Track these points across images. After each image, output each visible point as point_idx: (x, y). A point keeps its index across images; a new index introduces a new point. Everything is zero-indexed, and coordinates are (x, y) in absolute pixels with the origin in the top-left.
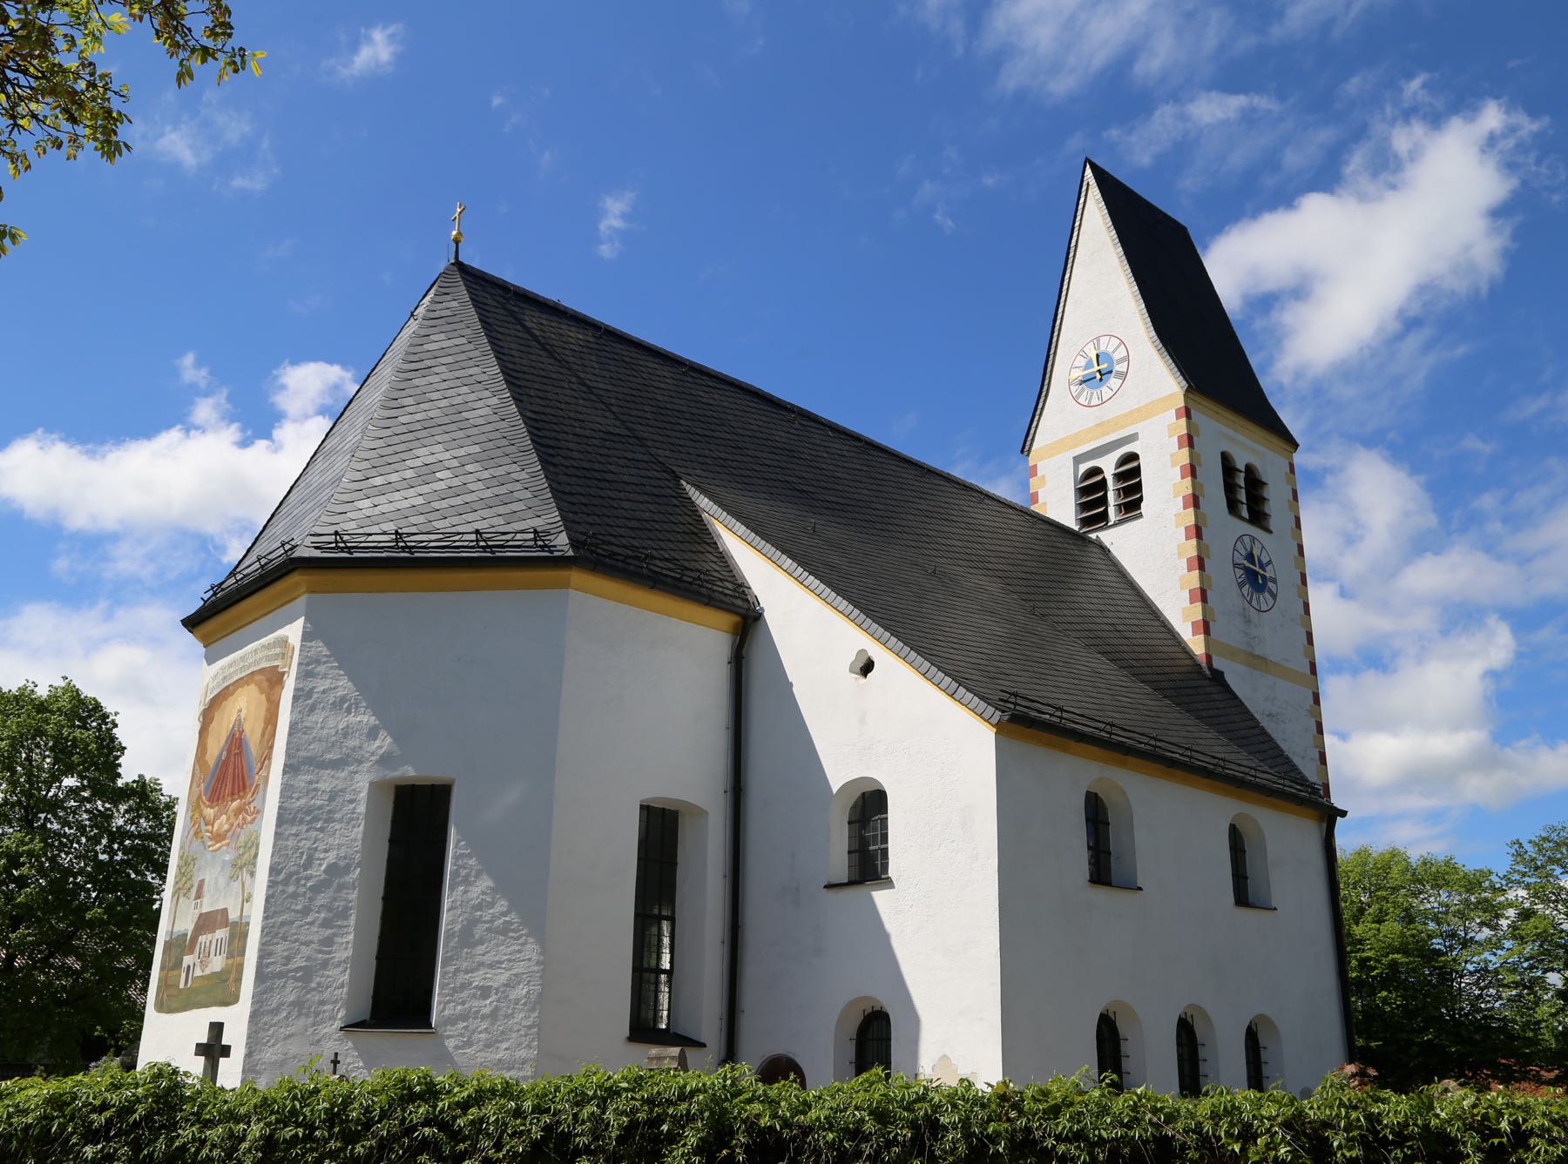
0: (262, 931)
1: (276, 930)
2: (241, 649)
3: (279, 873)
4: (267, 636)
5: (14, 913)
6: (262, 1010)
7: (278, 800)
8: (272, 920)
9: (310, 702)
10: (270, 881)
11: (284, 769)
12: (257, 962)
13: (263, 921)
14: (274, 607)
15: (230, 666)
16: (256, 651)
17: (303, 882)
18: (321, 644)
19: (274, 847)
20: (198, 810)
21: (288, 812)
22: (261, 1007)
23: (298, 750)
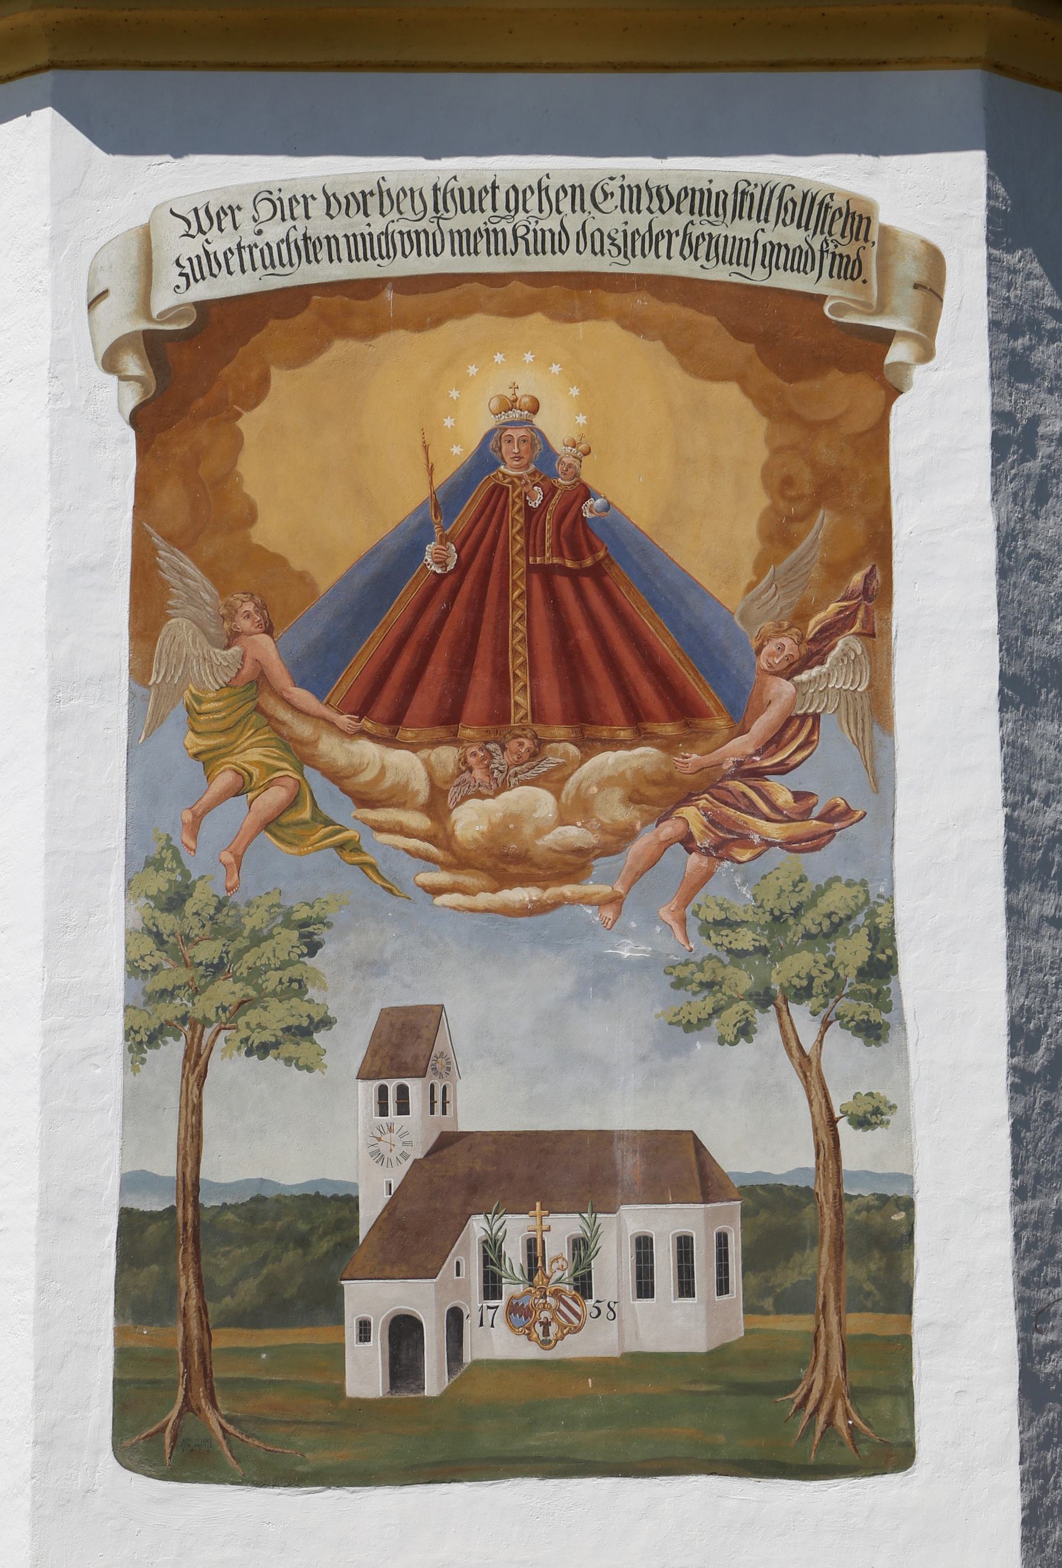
0: (1017, 1237)
1: (1046, 1234)
2: (429, 157)
3: (1032, 1047)
4: (438, 157)
5: (633, 925)
6: (1047, 1502)
7: (999, 796)
8: (1037, 1203)
9: (1033, 466)
10: (1014, 1070)
11: (1001, 692)
12: (1020, 1340)
13: (1013, 1203)
14: (25, 66)
15: (360, 202)
16: (517, 196)
17: (527, 1331)
18: (1036, 267)
19: (1009, 957)
20: (455, 861)
21: (1029, 841)
22: (1044, 1490)
23: (1027, 632)
